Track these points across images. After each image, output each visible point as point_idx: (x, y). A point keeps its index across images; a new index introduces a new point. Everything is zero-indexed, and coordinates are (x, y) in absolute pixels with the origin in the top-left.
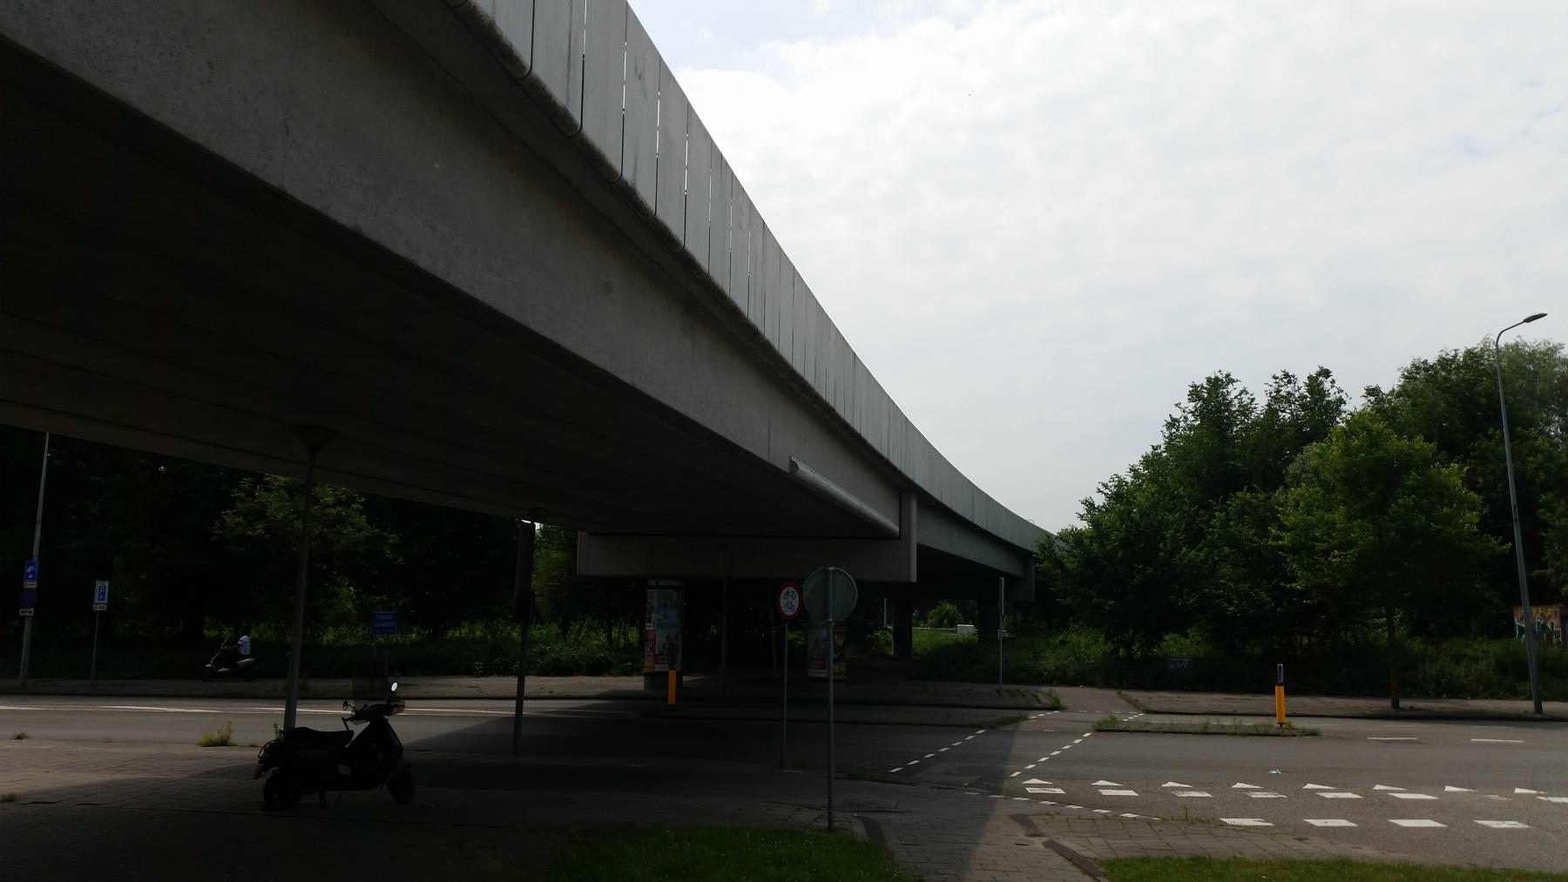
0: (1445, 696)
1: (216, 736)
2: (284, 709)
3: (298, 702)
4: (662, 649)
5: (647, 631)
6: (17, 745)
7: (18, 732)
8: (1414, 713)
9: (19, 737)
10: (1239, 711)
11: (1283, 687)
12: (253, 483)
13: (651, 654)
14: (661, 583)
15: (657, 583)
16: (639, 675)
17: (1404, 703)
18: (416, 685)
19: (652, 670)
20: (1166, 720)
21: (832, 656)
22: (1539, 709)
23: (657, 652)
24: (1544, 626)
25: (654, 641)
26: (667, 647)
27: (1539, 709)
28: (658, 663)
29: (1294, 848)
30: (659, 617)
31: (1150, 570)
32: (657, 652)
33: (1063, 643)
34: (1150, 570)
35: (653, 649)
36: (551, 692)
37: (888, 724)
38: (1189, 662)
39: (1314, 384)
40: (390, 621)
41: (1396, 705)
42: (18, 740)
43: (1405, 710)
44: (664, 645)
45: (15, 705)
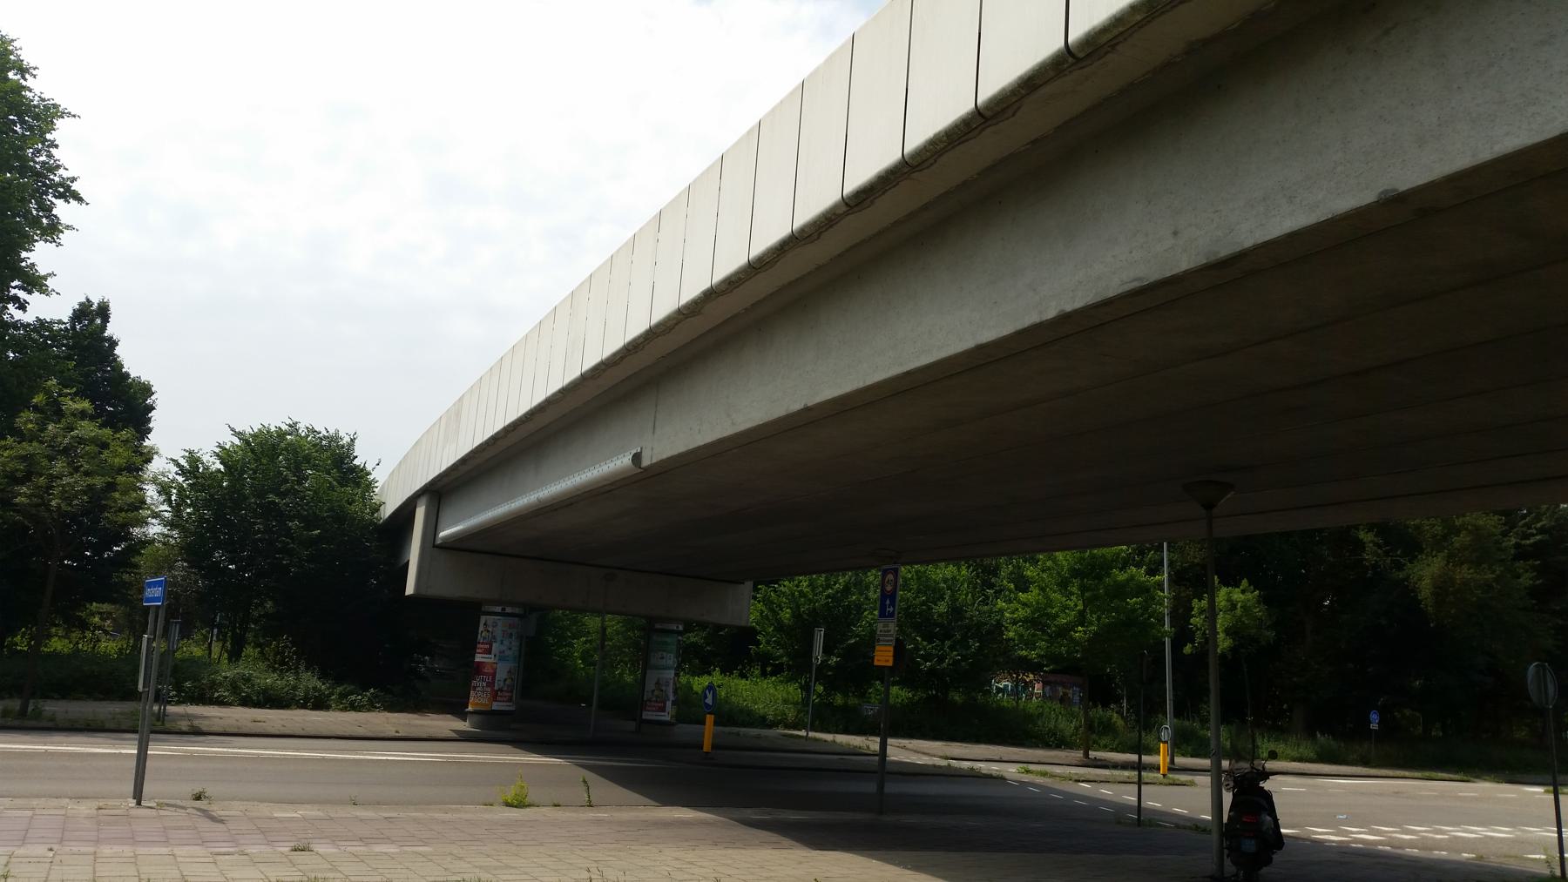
2: (136, 752)
3: (152, 736)
4: (502, 683)
6: (515, 814)
7: (198, 789)
8: (1099, 763)
10: (1004, 759)
14: (509, 610)
15: (503, 609)
17: (1092, 754)
19: (489, 709)
23: (496, 688)
25: (494, 675)
26: (507, 682)
29: (424, 859)
32: (496, 688)
35: (491, 684)
37: (927, 775)
39: (219, 446)
41: (1086, 754)
44: (505, 680)
45: (476, 753)
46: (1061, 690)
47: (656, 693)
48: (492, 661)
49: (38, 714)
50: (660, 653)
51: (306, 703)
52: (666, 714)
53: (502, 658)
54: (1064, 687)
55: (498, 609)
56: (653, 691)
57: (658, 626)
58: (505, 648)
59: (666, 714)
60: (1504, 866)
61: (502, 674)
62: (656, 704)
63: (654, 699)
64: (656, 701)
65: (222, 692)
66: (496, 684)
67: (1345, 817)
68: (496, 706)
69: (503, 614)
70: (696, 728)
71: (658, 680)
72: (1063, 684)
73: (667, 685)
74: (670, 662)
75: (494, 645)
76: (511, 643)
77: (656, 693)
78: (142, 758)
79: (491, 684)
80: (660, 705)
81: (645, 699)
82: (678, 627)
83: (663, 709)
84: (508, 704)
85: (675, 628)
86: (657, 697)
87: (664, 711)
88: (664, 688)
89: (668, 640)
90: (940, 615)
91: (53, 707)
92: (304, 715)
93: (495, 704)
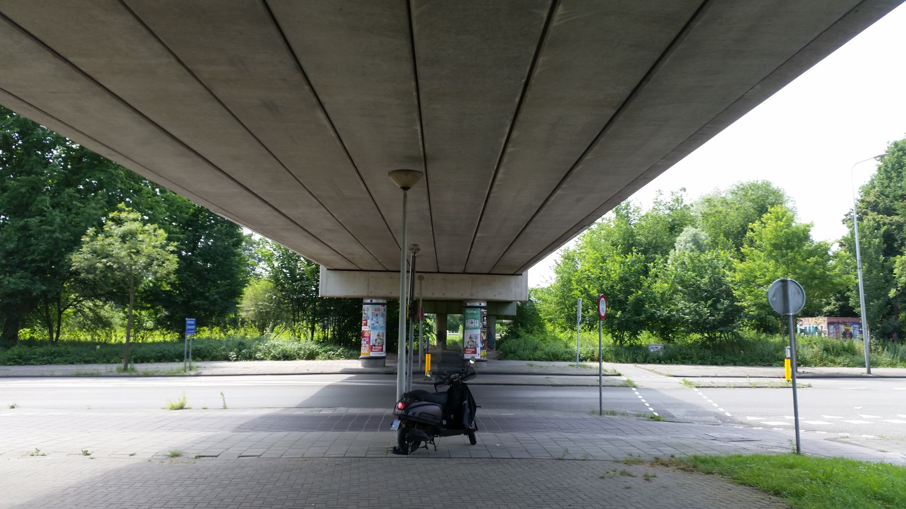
0: (802, 366)
1: (177, 403)
4: (374, 342)
5: (363, 331)
7: (11, 404)
9: (13, 407)
10: (718, 375)
11: (789, 360)
12: (95, 232)
13: (368, 345)
14: (374, 301)
15: (371, 301)
16: (357, 359)
18: (205, 367)
19: (368, 356)
20: (753, 380)
21: (480, 345)
22: (869, 372)
24: (816, 328)
26: (378, 341)
27: (869, 372)
28: (372, 351)
30: (373, 322)
31: (640, 292)
32: (371, 344)
33: (214, 344)
34: (640, 292)
35: (368, 342)
36: (308, 370)
38: (661, 348)
40: (192, 325)
42: (12, 409)
43: (800, 373)
44: (376, 340)
46: (842, 328)
47: (470, 343)
48: (368, 330)
49: (133, 370)
50: (470, 320)
51: (303, 357)
52: (477, 355)
53: (374, 328)
54: (846, 325)
55: (369, 301)
56: (468, 342)
57: (468, 304)
58: (374, 322)
59: (477, 355)
60: (192, 439)
61: (374, 337)
62: (470, 350)
63: (377, 344)
64: (470, 348)
65: (258, 355)
66: (371, 342)
67: (860, 407)
68: (372, 354)
69: (371, 304)
70: (395, 364)
71: (471, 336)
72: (845, 324)
73: (476, 337)
74: (477, 325)
75: (368, 321)
76: (377, 319)
77: (470, 343)
78: (791, 387)
79: (368, 342)
80: (472, 350)
81: (465, 347)
82: (480, 304)
83: (475, 352)
84: (380, 353)
85: (479, 305)
86: (471, 345)
87: (476, 353)
88: (474, 340)
89: (475, 312)
90: (705, 284)
91: (141, 367)
92: (351, 363)
93: (371, 353)
